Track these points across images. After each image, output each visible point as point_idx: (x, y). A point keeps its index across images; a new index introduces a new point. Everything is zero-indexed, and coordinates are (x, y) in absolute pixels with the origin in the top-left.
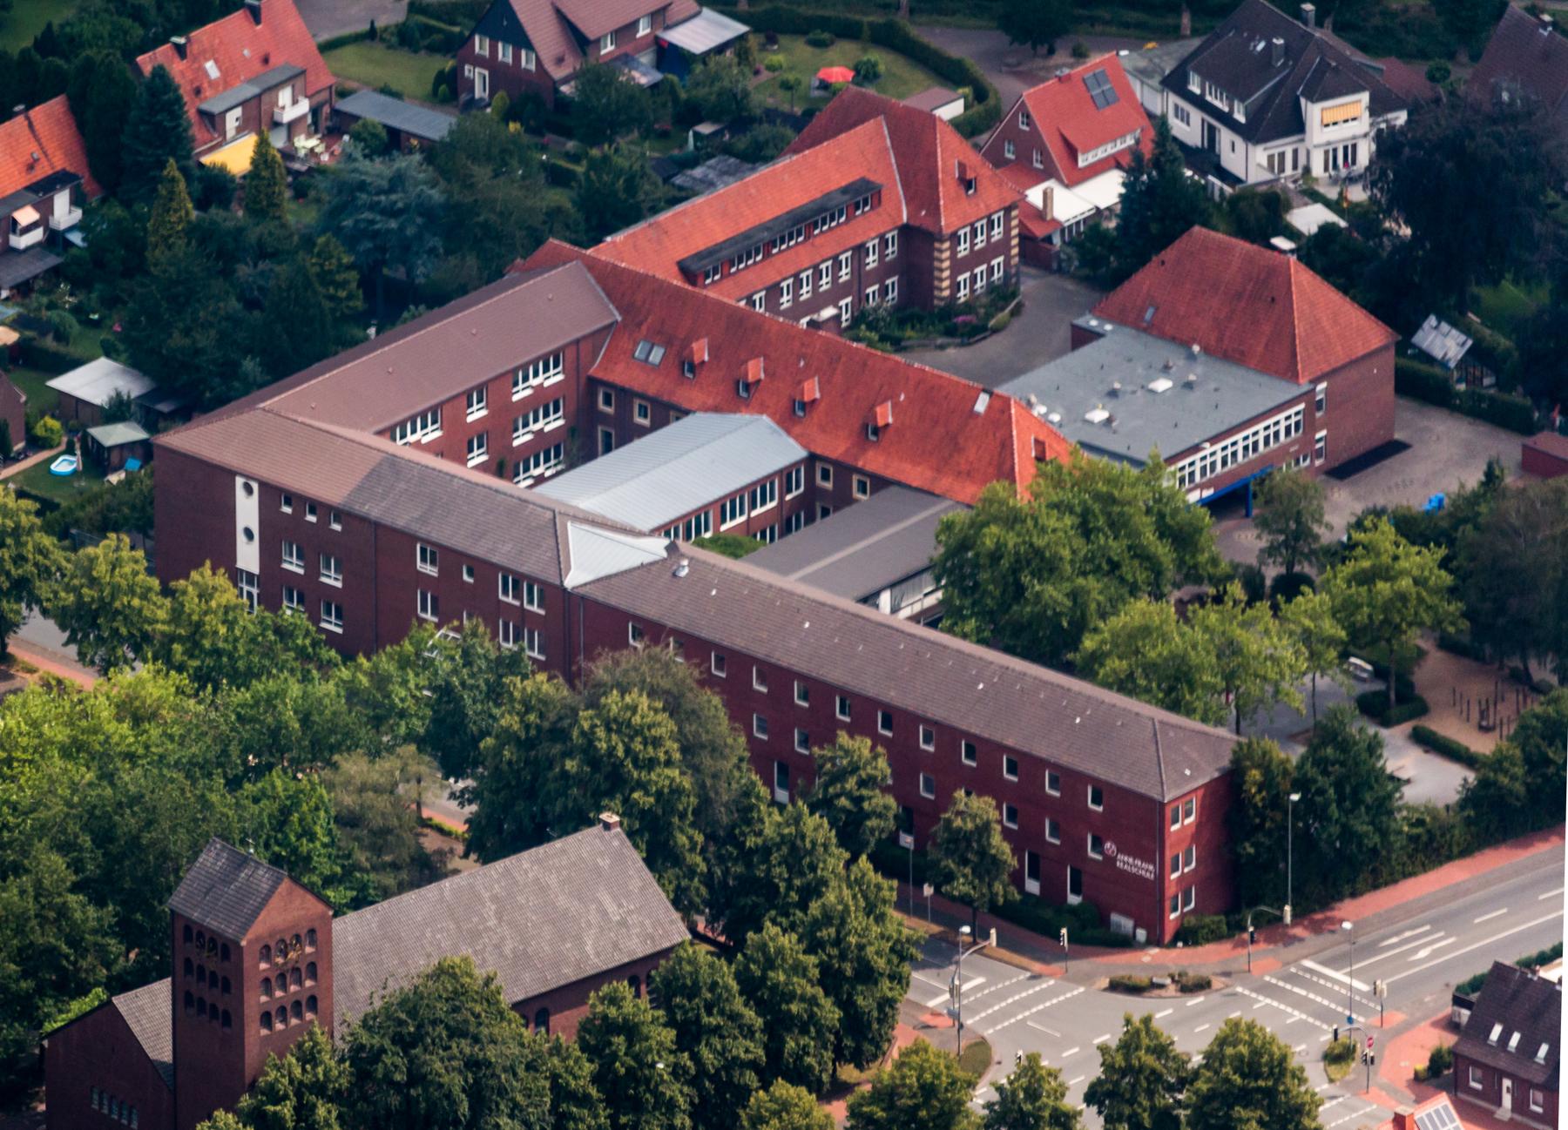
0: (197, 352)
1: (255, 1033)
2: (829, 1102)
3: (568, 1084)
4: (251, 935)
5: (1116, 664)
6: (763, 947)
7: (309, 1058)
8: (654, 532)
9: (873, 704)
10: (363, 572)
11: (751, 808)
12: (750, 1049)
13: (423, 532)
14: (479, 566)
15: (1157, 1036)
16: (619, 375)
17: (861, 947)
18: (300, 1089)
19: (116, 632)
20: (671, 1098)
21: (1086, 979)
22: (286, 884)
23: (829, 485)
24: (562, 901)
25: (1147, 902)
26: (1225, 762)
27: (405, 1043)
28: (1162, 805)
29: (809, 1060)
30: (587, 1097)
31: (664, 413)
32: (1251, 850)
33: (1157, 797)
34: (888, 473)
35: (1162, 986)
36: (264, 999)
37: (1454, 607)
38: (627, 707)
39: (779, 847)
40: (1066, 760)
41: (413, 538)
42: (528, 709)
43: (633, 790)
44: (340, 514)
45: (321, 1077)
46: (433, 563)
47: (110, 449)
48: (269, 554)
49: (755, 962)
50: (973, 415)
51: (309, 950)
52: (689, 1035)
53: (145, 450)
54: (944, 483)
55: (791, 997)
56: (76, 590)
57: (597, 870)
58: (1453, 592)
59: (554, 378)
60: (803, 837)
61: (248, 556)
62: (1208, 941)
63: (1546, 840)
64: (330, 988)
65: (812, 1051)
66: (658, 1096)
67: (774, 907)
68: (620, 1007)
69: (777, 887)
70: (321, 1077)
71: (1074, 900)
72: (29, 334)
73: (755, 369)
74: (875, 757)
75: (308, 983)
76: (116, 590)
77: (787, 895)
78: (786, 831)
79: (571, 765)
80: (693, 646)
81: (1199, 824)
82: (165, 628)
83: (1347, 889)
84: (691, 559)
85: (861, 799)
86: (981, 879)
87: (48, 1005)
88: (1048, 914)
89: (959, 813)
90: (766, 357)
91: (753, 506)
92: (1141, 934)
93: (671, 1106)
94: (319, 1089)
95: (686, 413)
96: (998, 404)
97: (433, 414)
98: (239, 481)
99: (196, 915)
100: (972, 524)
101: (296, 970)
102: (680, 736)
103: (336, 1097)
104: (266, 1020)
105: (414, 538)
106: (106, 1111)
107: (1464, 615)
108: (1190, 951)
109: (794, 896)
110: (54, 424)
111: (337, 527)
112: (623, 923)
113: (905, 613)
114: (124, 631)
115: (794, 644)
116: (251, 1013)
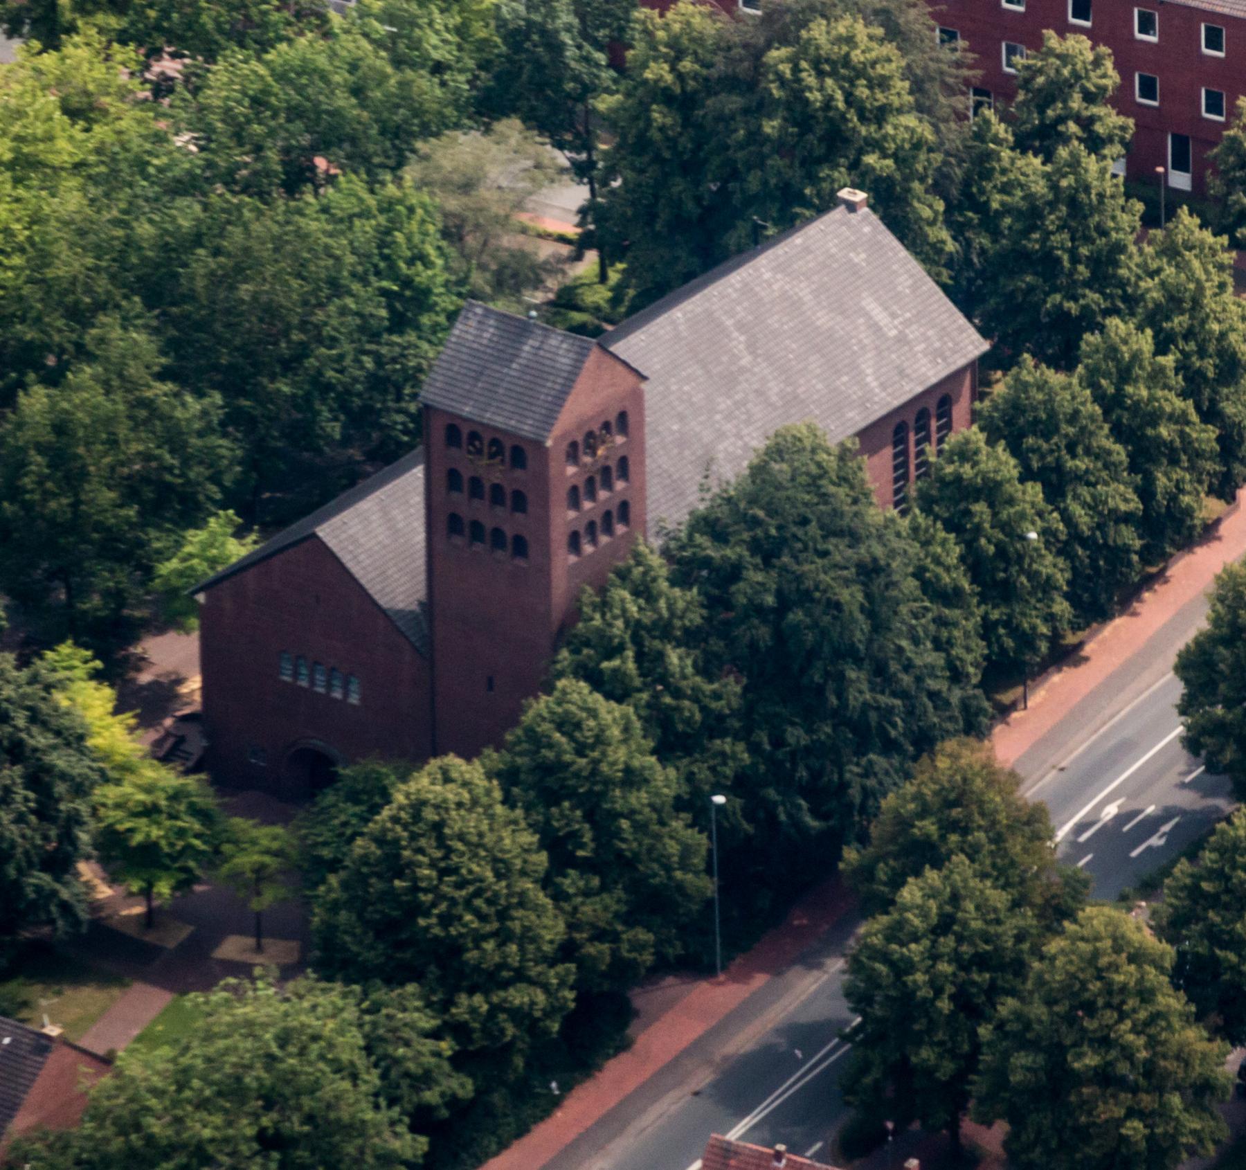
1: (563, 561)
3: (937, 577)
7: (644, 591)
11: (990, 156)
17: (1223, 335)
18: (636, 629)
20: (1049, 578)
24: (823, 319)
27: (767, 552)
36: (572, 514)
38: (840, 40)
42: (680, 54)
45: (665, 613)
49: (1107, 375)
51: (620, 440)
52: (1056, 484)
55: (1154, 418)
57: (854, 270)
60: (1087, 189)
64: (642, 489)
65: (1188, 487)
66: (1033, 576)
67: (1055, 289)
68: (975, 464)
69: (1058, 260)
70: (665, 613)
74: (1097, 63)
75: (620, 485)
77: (1073, 271)
78: (1064, 183)
79: (770, 127)
85: (1092, 120)
93: (1046, 587)
94: (664, 630)
99: (467, 410)
101: (606, 470)
103: (690, 638)
104: (574, 542)
106: (304, 683)
109: (1083, 271)
112: (901, 339)
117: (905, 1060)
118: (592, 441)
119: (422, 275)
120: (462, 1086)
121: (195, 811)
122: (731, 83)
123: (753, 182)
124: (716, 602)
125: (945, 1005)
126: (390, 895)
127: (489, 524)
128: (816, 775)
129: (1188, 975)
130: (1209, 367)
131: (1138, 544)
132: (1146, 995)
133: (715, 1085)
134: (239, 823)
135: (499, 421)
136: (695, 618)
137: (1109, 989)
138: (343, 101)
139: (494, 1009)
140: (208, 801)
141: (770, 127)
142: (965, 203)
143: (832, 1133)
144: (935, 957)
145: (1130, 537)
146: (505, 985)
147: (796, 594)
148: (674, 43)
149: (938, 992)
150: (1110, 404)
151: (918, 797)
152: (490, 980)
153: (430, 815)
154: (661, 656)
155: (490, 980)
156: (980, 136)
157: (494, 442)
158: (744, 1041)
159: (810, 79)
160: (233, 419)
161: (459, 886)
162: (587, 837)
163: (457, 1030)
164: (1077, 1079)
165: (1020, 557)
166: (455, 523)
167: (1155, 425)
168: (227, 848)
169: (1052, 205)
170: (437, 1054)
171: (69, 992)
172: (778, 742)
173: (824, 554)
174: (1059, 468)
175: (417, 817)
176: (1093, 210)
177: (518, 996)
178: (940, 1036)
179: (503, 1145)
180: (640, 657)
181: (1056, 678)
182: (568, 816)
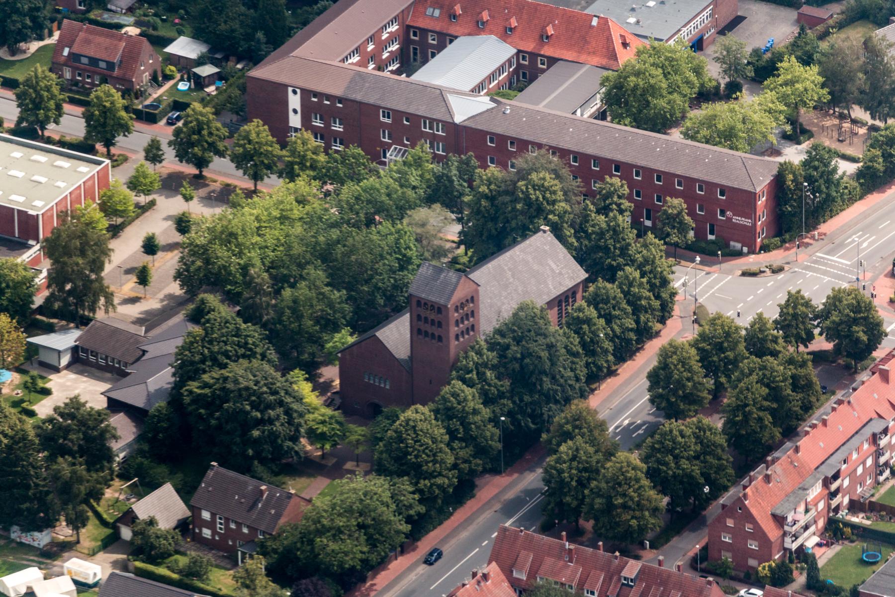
0: (233, 31)
1: (454, 343)
4: (452, 302)
5: (705, 132)
6: (627, 277)
7: (479, 353)
8: (477, 89)
9: (611, 161)
10: (356, 126)
12: (630, 323)
13: (383, 104)
14: (409, 117)
15: (803, 298)
16: (421, 23)
17: (662, 272)
19: (262, 162)
21: (730, 272)
22: (464, 278)
23: (526, 63)
25: (748, 236)
26: (775, 172)
27: (518, 341)
28: (755, 194)
29: (650, 324)
30: (578, 353)
31: (445, 40)
32: (789, 209)
33: (751, 189)
34: (556, 56)
35: (764, 272)
36: (456, 328)
37: (825, 91)
39: (608, 231)
40: (706, 178)
41: (378, 107)
43: (548, 214)
46: (389, 118)
47: (204, 78)
50: (591, 27)
51: (471, 305)
53: (219, 77)
54: (582, 58)
56: (243, 146)
58: (823, 86)
59: (394, 28)
60: (619, 226)
62: (774, 249)
63: (890, 188)
64: (478, 320)
66: (602, 348)
71: (711, 237)
72: (144, 29)
73: (485, 16)
74: (622, 186)
75: (471, 319)
79: (519, 206)
80: (555, 150)
81: (767, 200)
82: (289, 159)
83: (822, 220)
84: (510, 105)
86: (680, 233)
87: (326, 337)
88: (703, 245)
89: (669, 207)
90: (489, 10)
91: (500, 75)
92: (745, 249)
93: (606, 351)
94: (485, 365)
95: (456, 37)
96: (602, 21)
97: (357, 50)
98: (290, 89)
99: (423, 296)
100: (620, 77)
101: (467, 315)
102: (562, 189)
105: (379, 107)
106: (372, 382)
107: (829, 93)
108: (767, 254)
110: (173, 68)
111: (315, 100)
112: (560, 273)
113: (586, 116)
114: (266, 162)
115: (568, 139)
116: (452, 335)
118: (462, 306)
119: (409, 253)
120: (422, 509)
121: (338, 422)
122: (506, 193)
123: (513, 224)
124: (502, 356)
126: (399, 449)
127: (430, 332)
129: (651, 474)
130: (657, 282)
131: (635, 338)
132: (637, 480)
133: (501, 509)
135: (433, 299)
136: (495, 361)
138: (384, 198)
139: (432, 485)
141: (519, 206)
142: (580, 230)
143: (539, 524)
145: (633, 336)
146: (435, 477)
148: (488, 180)
149: (572, 479)
150: (626, 294)
151: (566, 418)
152: (431, 475)
153: (411, 423)
154: (484, 373)
155: (431, 475)
156: (585, 209)
158: (510, 495)
159: (531, 191)
160: (350, 298)
161: (421, 446)
162: (461, 430)
163: (421, 491)
164: (616, 507)
165: (598, 342)
166: (419, 331)
167: (640, 300)
168: (347, 434)
169: (608, 231)
170: (414, 499)
171: (298, 479)
172: (521, 400)
173: (536, 341)
174: (610, 314)
175: (407, 424)
176: (621, 232)
177: (439, 481)
178: (572, 493)
179: (435, 528)
180: (478, 374)
181: (609, 380)
182: (455, 424)
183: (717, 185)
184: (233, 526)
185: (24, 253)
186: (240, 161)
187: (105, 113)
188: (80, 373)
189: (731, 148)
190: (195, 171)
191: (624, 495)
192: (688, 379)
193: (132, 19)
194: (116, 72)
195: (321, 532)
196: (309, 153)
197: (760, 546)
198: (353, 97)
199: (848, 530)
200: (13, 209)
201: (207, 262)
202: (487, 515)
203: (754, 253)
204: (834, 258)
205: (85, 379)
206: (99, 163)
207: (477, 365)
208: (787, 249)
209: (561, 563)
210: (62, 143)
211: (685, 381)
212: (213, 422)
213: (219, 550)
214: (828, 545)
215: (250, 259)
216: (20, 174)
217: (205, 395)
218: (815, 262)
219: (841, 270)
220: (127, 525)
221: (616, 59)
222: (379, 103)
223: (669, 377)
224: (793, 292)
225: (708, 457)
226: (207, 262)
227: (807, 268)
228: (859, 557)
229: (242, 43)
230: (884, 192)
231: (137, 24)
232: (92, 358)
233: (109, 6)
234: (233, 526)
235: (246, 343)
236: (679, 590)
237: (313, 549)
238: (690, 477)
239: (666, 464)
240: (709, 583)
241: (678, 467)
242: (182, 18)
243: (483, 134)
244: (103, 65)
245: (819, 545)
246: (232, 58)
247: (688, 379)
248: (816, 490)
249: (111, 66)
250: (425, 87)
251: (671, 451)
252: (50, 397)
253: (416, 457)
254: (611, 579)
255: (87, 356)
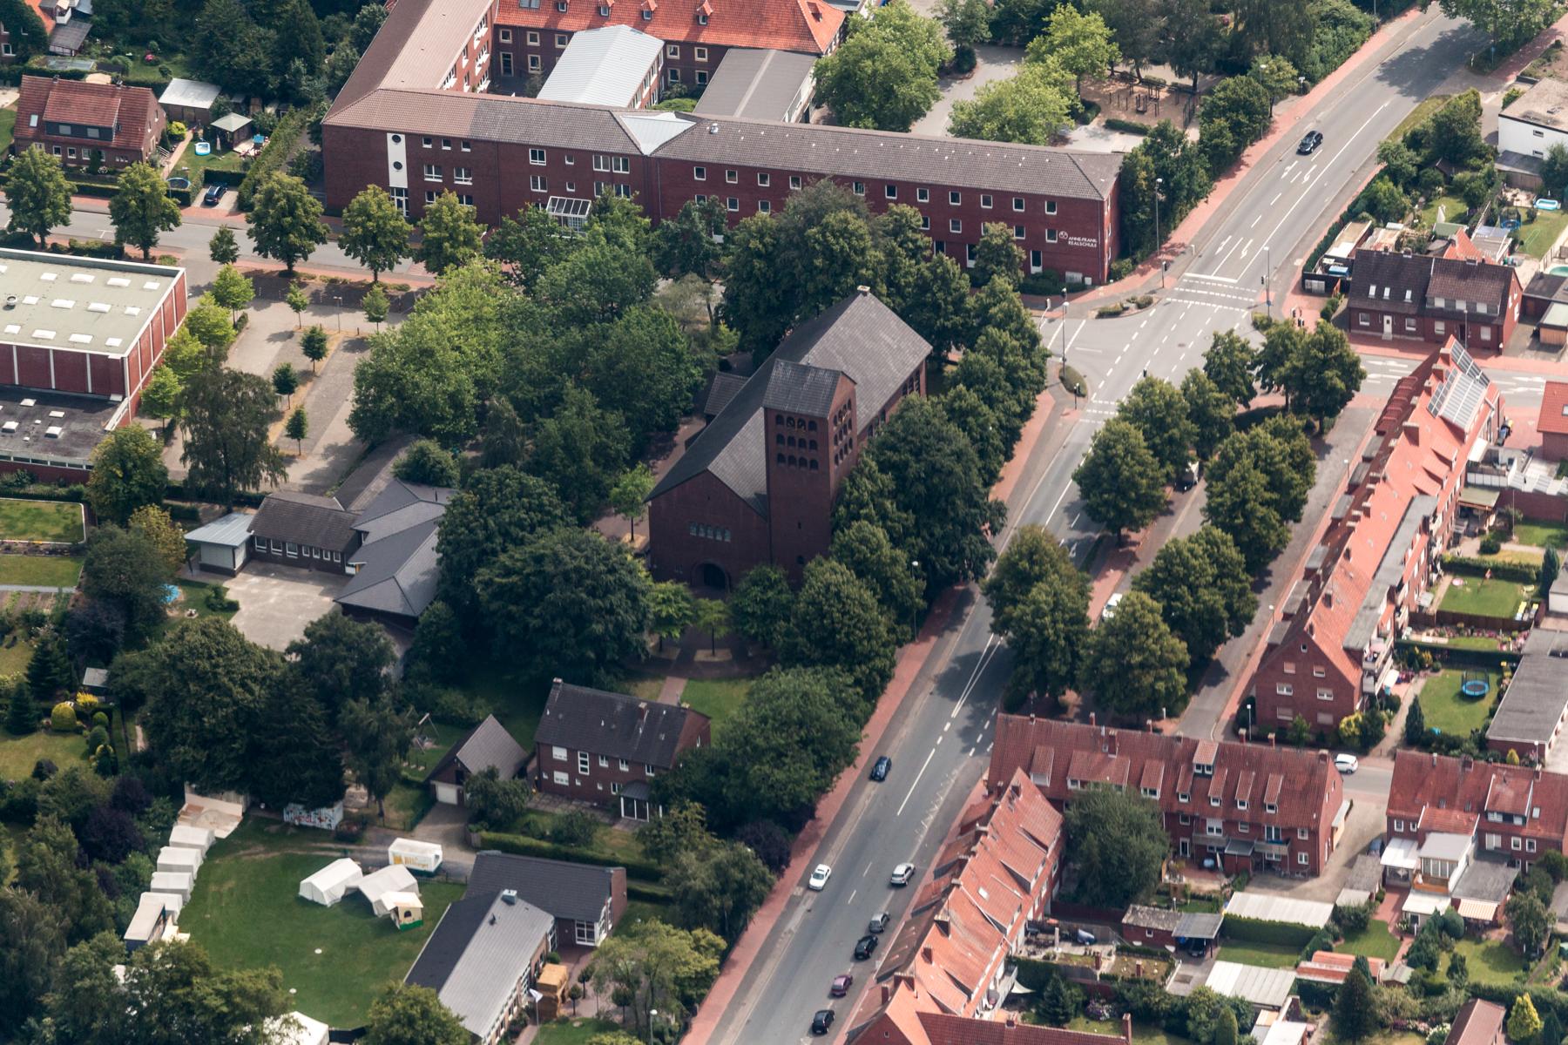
0: (256, 63)
2: (142, 417)
9: (882, 182)
13: (532, 141)
19: (390, 243)
21: (1080, 315)
27: (917, 454)
34: (723, 42)
41: (525, 147)
44: (467, 143)
46: (542, 158)
48: (414, 173)
53: (250, 131)
54: (762, 41)
56: (362, 224)
58: (1110, 41)
61: (398, 179)
76: (384, 218)
92: (1088, 281)
94: (881, 493)
98: (390, 136)
109: (951, 308)
110: (181, 125)
112: (899, 348)
117: (1044, 668)
118: (841, 414)
119: (679, 347)
121: (685, 599)
122: (791, 244)
124: (901, 479)
125: (1062, 642)
127: (798, 457)
128: (947, 547)
132: (1156, 626)
134: (704, 602)
135: (803, 411)
136: (892, 486)
137: (1142, 625)
138: (619, 275)
139: (872, 670)
140: (688, 594)
141: (818, 262)
143: (999, 703)
144: (1054, 622)
147: (934, 470)
148: (759, 231)
154: (883, 505)
157: (790, 419)
158: (941, 666)
160: (628, 422)
161: (851, 619)
164: (1130, 667)
166: (781, 458)
169: (935, 280)
172: (932, 535)
183: (1043, 197)
184: (604, 764)
185: (111, 415)
186: (352, 246)
187: (143, 201)
188: (263, 573)
189: (1029, 142)
190: (284, 267)
191: (1141, 650)
192: (1141, 475)
193: (91, 64)
194: (114, 141)
195: (758, 754)
196: (461, 223)
197: (1336, 695)
198: (485, 135)
199: (1427, 655)
200: (84, 355)
201: (400, 395)
202: (922, 702)
203: (1101, 284)
204: (1212, 277)
205: (274, 582)
206: (172, 274)
207: (871, 493)
208: (1143, 273)
209: (1099, 757)
210: (74, 250)
211: (1138, 478)
212: (534, 623)
213: (583, 799)
214: (1407, 680)
215: (459, 382)
216: (70, 304)
217: (514, 584)
218: (1190, 286)
219: (1229, 291)
220: (447, 781)
221: (811, 38)
222: (525, 140)
223: (1115, 476)
224: (1222, 333)
225: (1226, 581)
226: (400, 395)
227: (1182, 295)
228: (1457, 690)
229: (271, 79)
230: (1233, 176)
231: (102, 68)
232: (276, 552)
233: (52, 49)
234: (604, 764)
235: (541, 505)
236: (1280, 772)
237: (744, 784)
238: (1212, 611)
239: (1178, 598)
240: (1323, 757)
241: (1197, 601)
242: (154, 52)
243: (684, 167)
244: (93, 133)
245: (1399, 682)
246: (255, 101)
247: (1141, 475)
248: (1383, 608)
249: (105, 133)
250: (547, 106)
251: (1183, 580)
252: (238, 614)
253: (847, 635)
254: (1176, 768)
255: (268, 549)
